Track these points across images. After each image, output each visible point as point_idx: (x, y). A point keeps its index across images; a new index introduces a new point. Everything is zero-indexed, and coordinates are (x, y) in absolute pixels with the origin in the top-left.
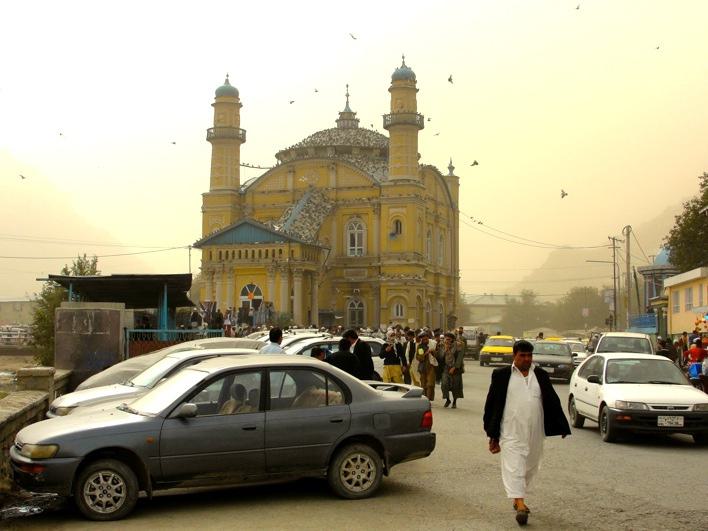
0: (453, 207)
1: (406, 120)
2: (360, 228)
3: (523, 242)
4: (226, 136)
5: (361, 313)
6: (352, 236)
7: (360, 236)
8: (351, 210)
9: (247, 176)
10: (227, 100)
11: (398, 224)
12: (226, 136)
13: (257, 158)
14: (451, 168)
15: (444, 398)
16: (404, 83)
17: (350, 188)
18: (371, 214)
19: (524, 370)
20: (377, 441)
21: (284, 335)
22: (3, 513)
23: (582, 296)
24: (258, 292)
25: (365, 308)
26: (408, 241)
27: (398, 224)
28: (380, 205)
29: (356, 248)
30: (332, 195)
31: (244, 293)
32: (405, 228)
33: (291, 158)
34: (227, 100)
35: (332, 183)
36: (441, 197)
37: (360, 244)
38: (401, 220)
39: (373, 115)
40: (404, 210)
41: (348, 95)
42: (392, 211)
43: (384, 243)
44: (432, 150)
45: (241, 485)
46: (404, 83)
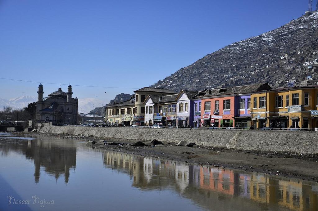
0: (77, 104)
1: (70, 93)
4: (41, 92)
9: (43, 100)
10: (41, 87)
11: (68, 108)
12: (41, 92)
13: (45, 96)
16: (70, 87)
22: (317, 61)
23: (112, 101)
26: (70, 111)
27: (68, 108)
33: (52, 96)
34: (41, 87)
36: (75, 103)
39: (65, 90)
44: (74, 96)
45: (169, 96)
46: (70, 87)
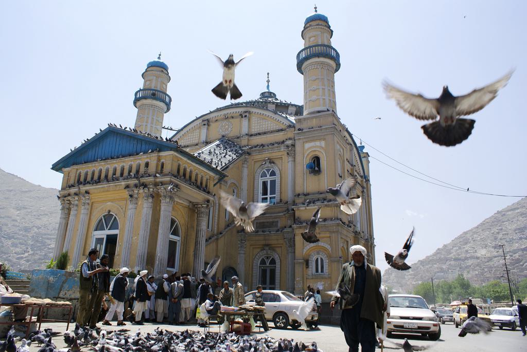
2: (273, 174)
3: (440, 183)
5: (273, 272)
6: (265, 184)
7: (273, 182)
8: (266, 155)
14: (361, 143)
15: (418, 327)
17: (259, 134)
18: (285, 157)
19: (444, 323)
20: (398, 269)
21: (58, 225)
24: (115, 226)
25: (278, 265)
28: (293, 145)
29: (269, 196)
30: (244, 142)
31: (99, 227)
32: (323, 163)
35: (245, 130)
37: (273, 192)
38: (320, 155)
40: (323, 143)
41: (268, 81)
42: (307, 145)
43: (299, 181)
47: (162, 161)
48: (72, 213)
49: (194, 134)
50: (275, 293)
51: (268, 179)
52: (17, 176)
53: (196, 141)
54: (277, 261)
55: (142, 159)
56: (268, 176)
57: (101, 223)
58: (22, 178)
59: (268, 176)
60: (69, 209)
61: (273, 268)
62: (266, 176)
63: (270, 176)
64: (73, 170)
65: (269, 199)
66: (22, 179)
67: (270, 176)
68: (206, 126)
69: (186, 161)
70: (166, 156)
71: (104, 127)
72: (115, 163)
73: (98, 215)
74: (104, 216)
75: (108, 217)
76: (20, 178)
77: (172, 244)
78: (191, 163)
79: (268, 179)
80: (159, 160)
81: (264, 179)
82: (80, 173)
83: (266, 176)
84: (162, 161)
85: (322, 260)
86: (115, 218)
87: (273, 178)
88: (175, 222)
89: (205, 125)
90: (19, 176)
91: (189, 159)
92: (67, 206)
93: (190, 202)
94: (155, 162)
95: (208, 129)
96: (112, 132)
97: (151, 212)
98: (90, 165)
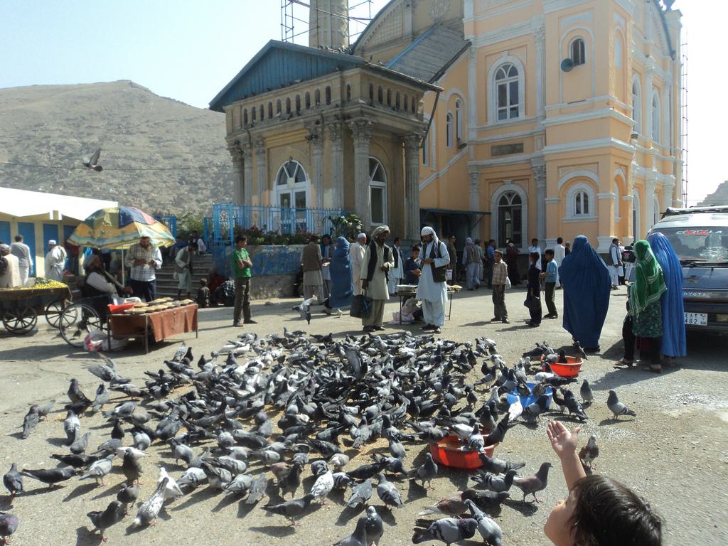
7: (514, 86)
47: (347, 84)
48: (246, 165)
49: (395, 22)
50: (166, 462)
51: (507, 81)
52: (174, 100)
53: (399, 33)
54: (522, 199)
55: (321, 85)
56: (506, 76)
57: (283, 174)
58: (181, 101)
59: (506, 76)
60: (242, 160)
61: (518, 209)
62: (504, 77)
63: (509, 76)
64: (235, 108)
65: (508, 111)
66: (182, 103)
67: (509, 76)
68: (410, 8)
69: (380, 79)
70: (351, 76)
71: (268, 41)
72: (287, 93)
73: (279, 165)
74: (286, 165)
75: (291, 167)
76: (179, 102)
77: (376, 193)
78: (388, 80)
79: (507, 81)
80: (343, 83)
81: (501, 82)
82: (246, 110)
83: (504, 77)
84: (347, 84)
85: (586, 196)
86: (299, 167)
87: (513, 79)
88: (376, 162)
89: (408, 6)
90: (177, 100)
91: (384, 76)
92: (239, 157)
93: (394, 134)
94: (339, 86)
95: (413, 12)
96: (274, 51)
97: (342, 156)
98: (257, 98)
